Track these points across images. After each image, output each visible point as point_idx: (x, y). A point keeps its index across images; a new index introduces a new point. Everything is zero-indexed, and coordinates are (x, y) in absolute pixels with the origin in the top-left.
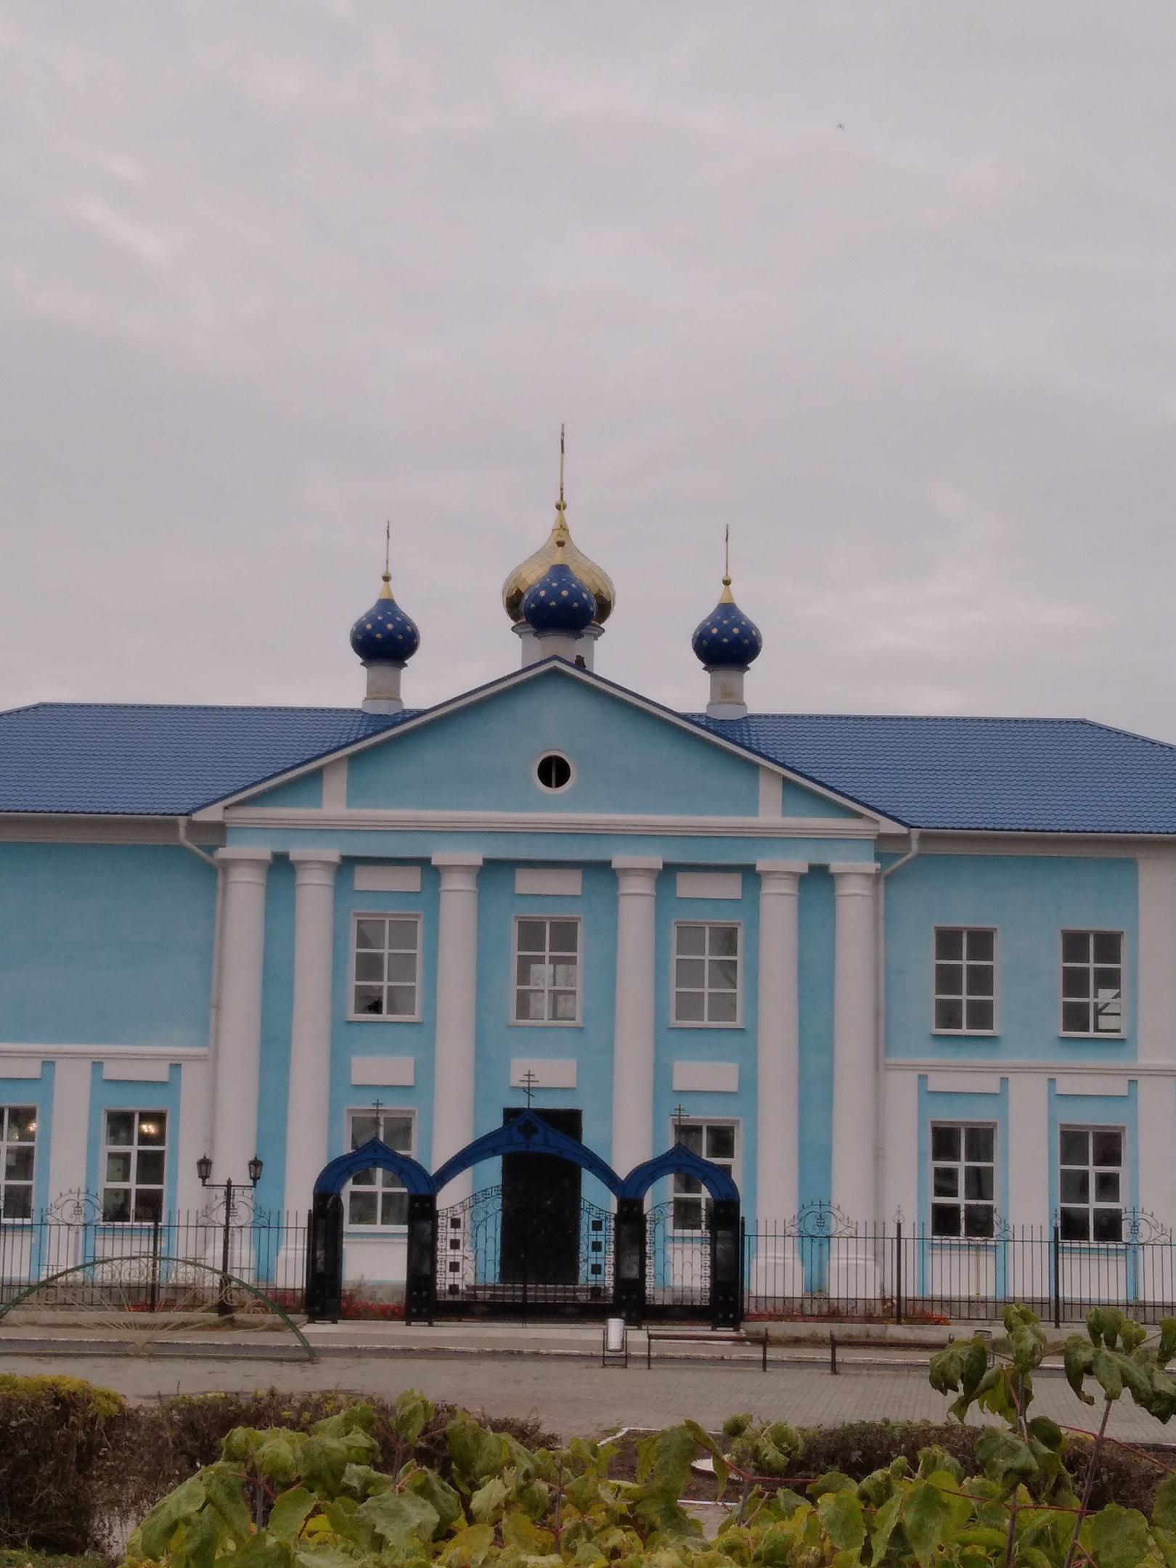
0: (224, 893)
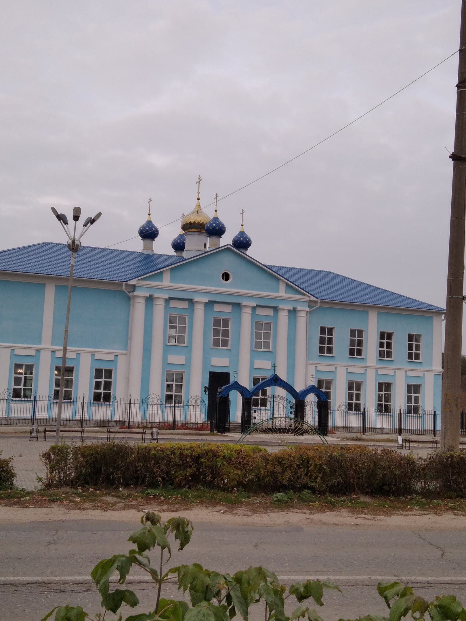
0: (133, 306)
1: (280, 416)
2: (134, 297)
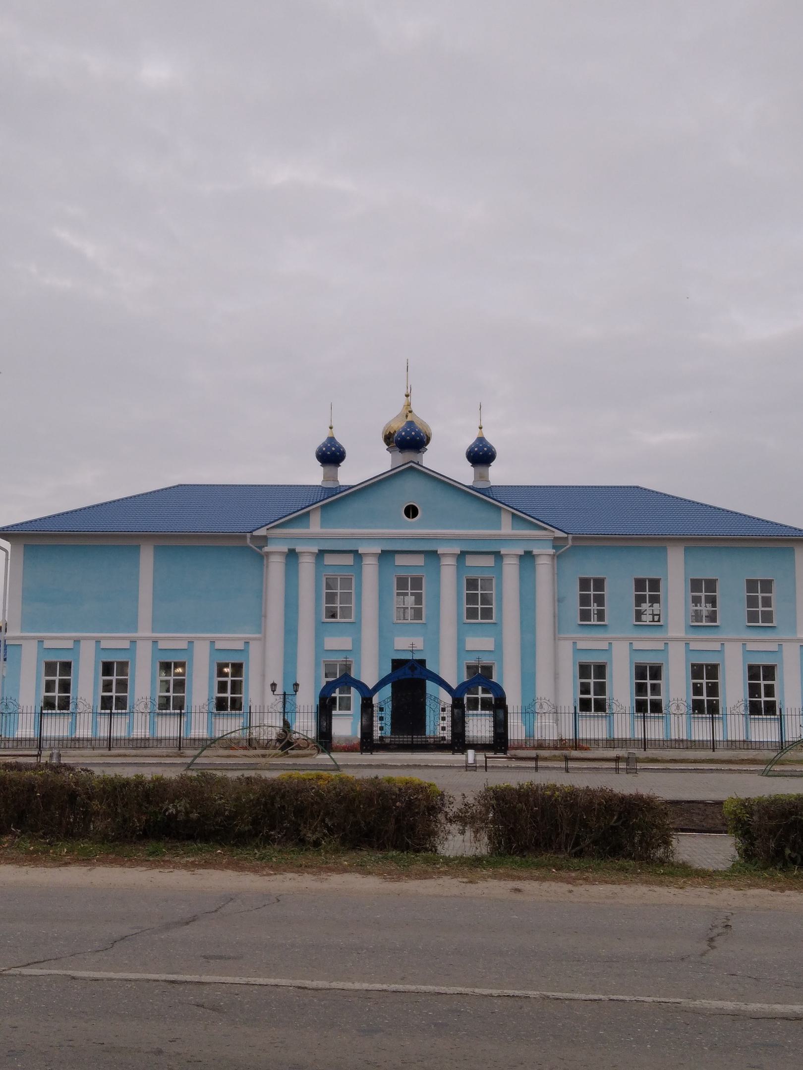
0: (267, 567)
1: (270, 723)
2: (268, 554)
